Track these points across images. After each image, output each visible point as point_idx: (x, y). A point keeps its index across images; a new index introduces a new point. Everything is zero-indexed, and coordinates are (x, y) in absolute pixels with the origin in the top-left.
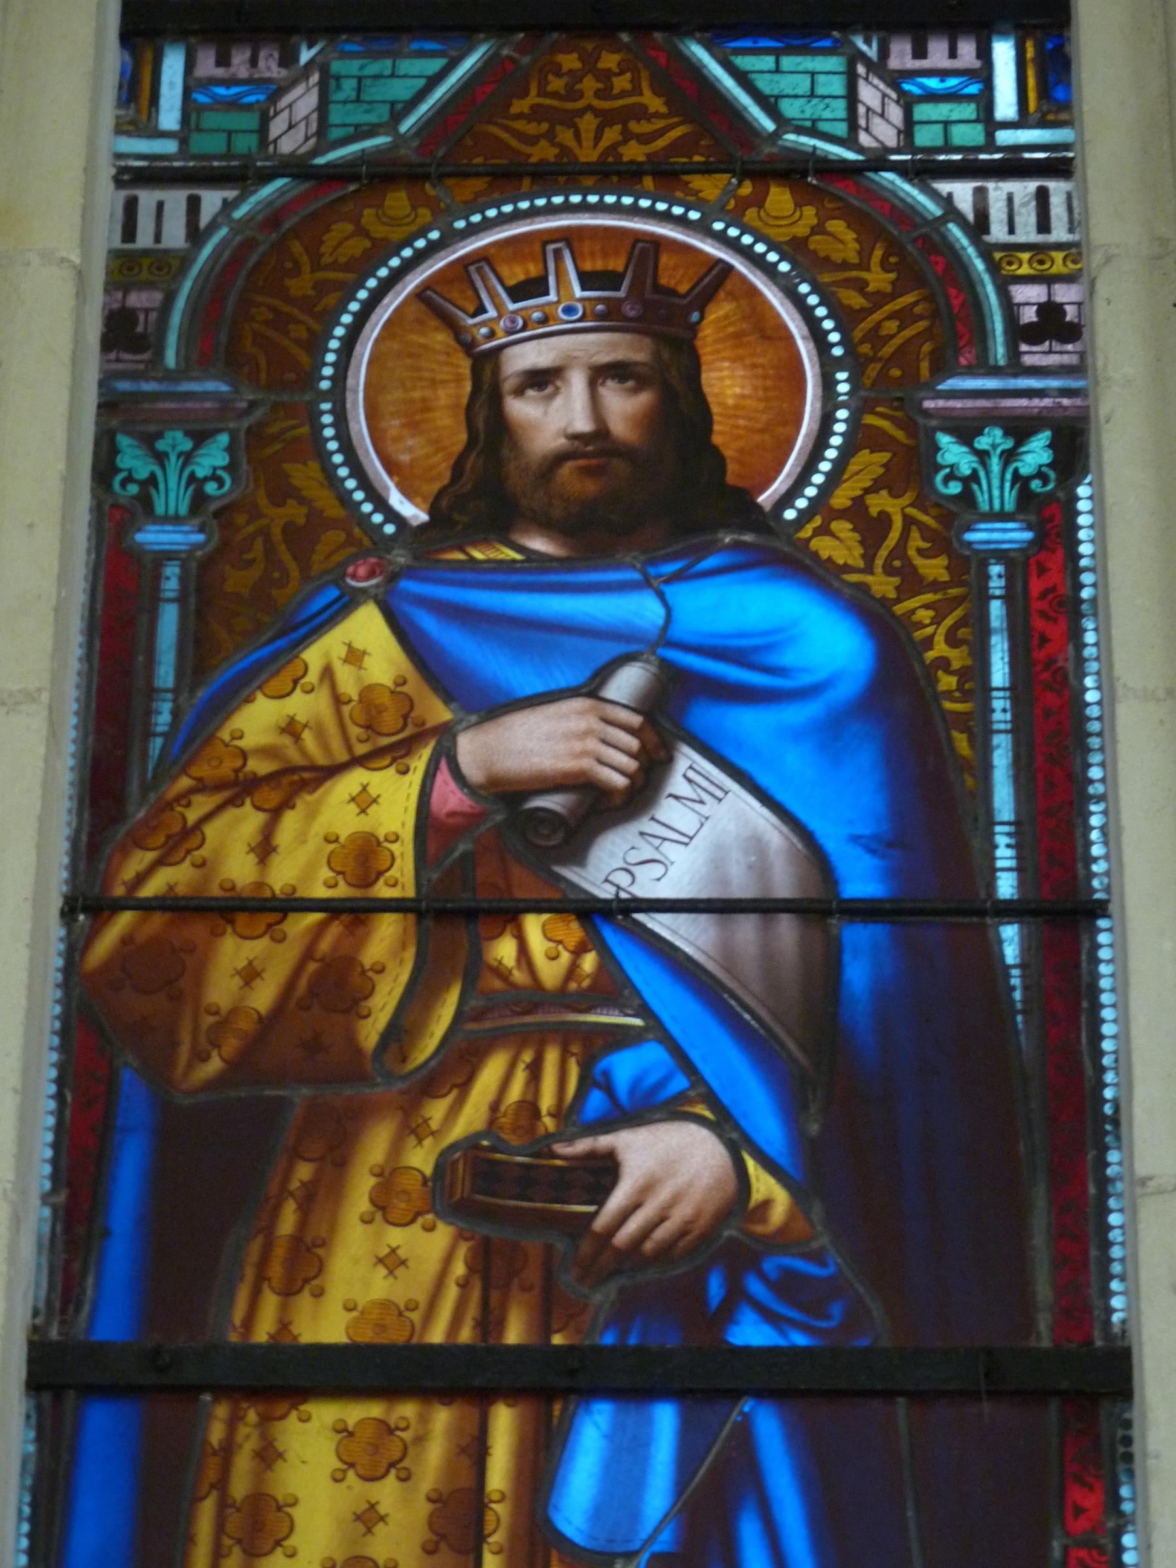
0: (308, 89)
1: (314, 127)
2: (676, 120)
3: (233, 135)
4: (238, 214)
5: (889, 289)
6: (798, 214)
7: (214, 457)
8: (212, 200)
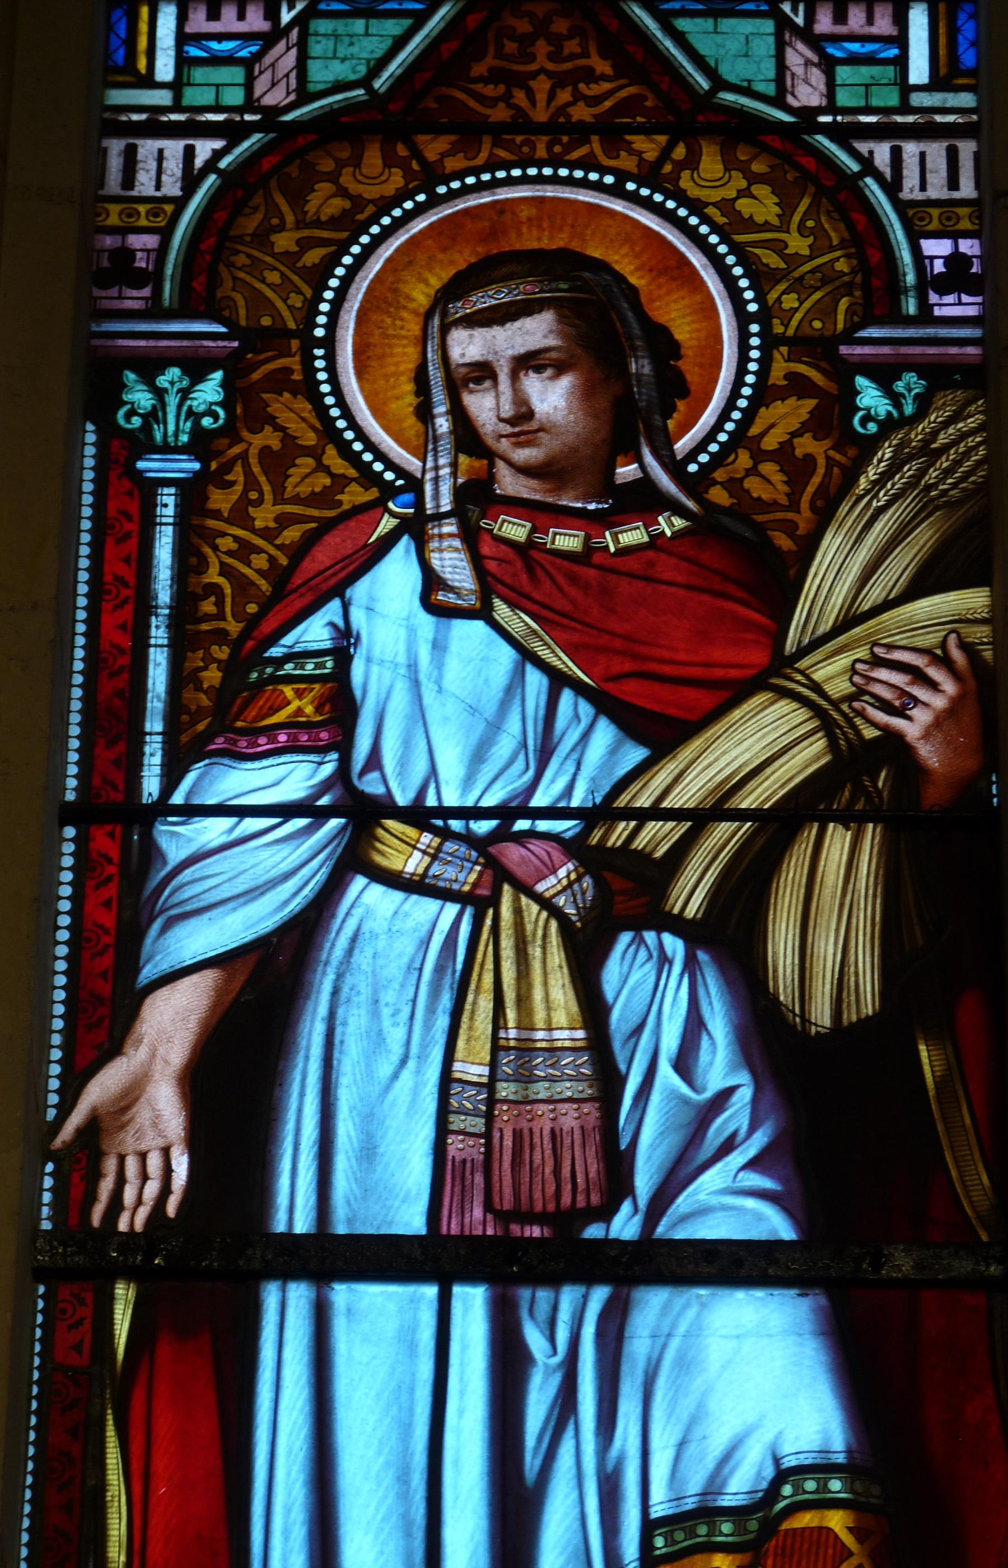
0: (288, 49)
1: (293, 83)
2: (622, 82)
3: (221, 88)
4: (223, 164)
5: (807, 252)
6: (727, 175)
7: (210, 391)
8: (205, 148)
